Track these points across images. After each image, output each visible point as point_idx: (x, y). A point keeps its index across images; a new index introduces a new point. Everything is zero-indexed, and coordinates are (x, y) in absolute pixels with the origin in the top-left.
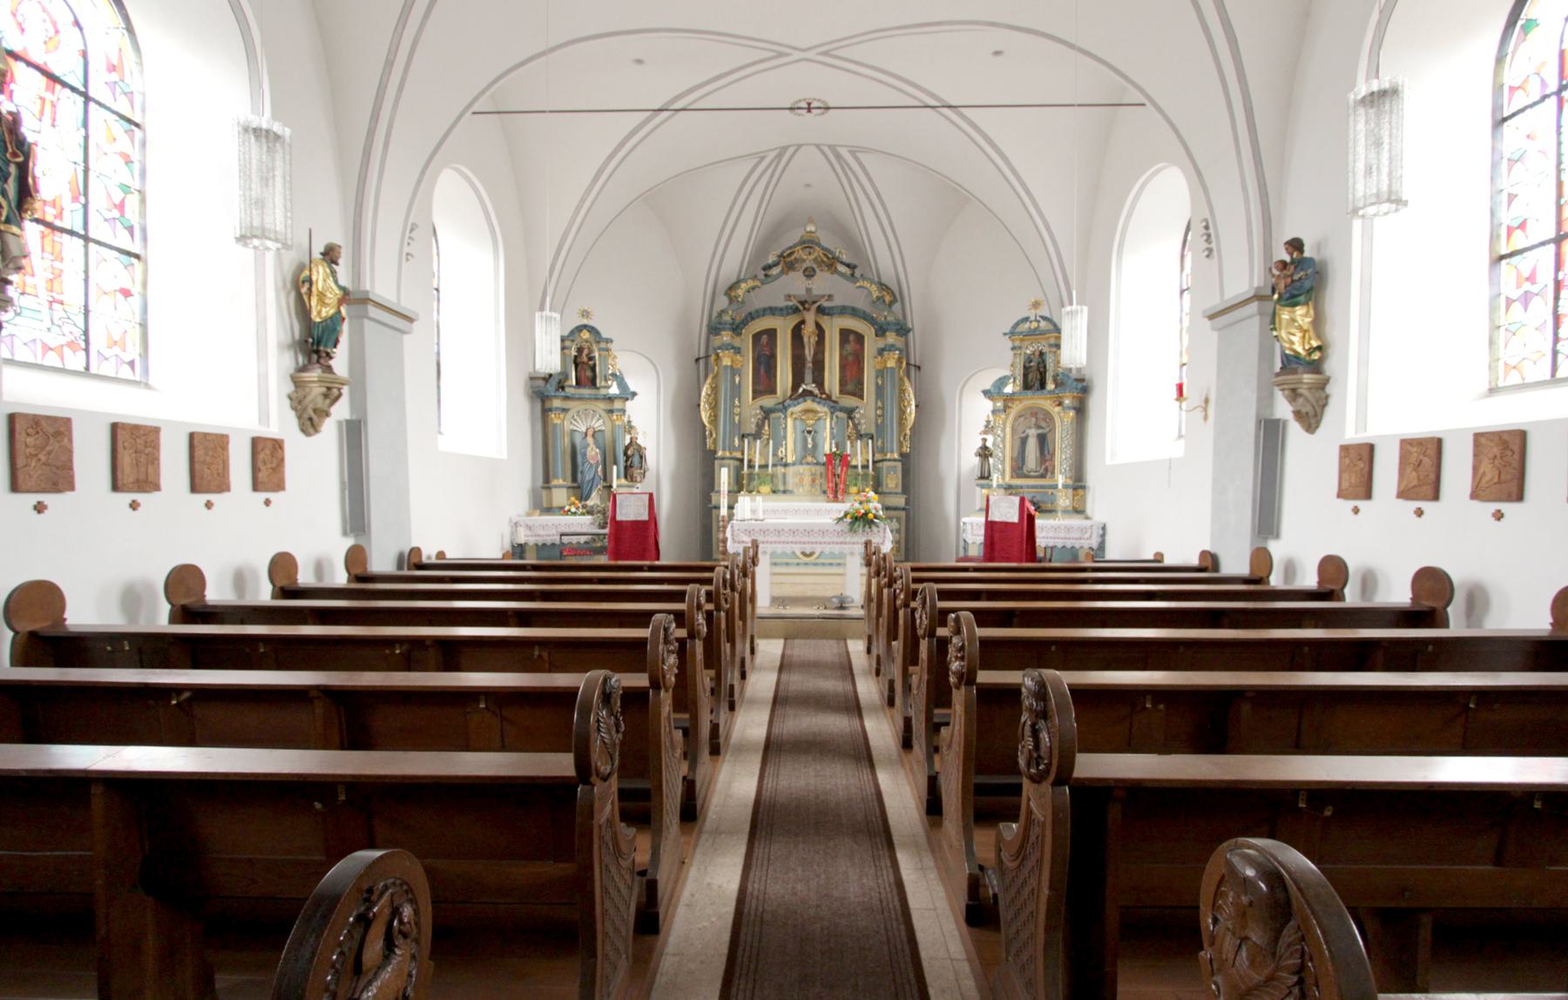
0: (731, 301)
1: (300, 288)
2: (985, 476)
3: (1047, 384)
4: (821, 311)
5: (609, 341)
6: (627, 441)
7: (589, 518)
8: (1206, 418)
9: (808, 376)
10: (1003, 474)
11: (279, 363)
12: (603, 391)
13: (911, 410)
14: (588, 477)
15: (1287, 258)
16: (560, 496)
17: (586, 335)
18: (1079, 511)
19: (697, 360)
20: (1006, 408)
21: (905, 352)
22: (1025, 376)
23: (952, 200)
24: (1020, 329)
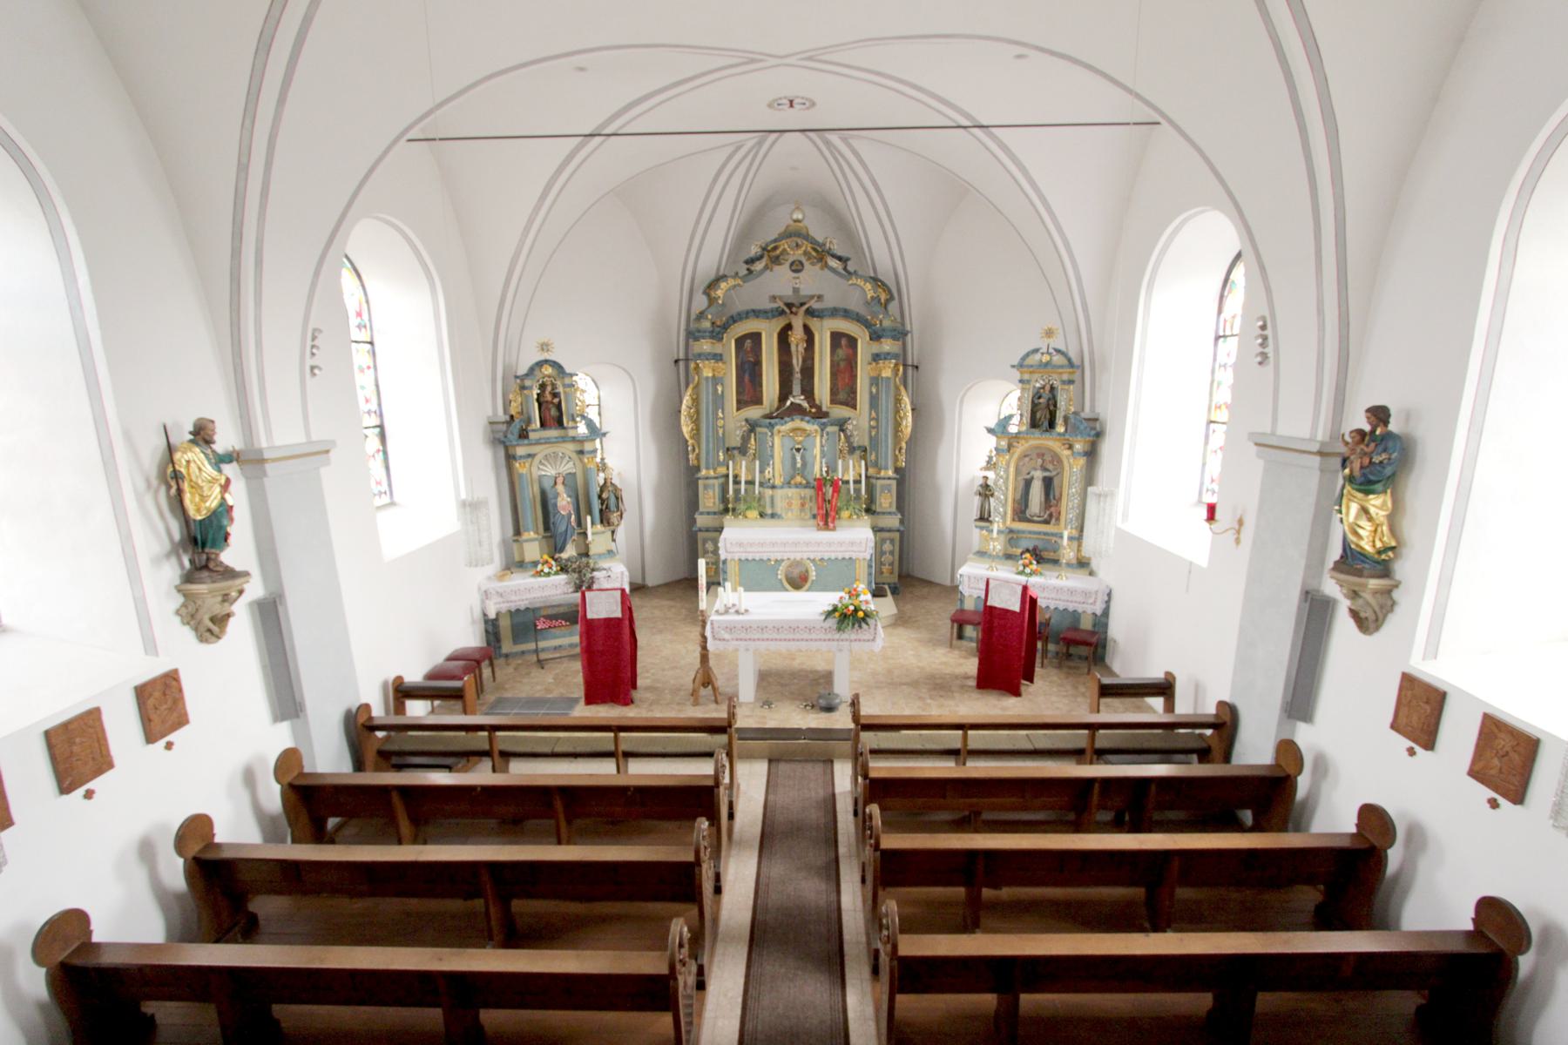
0: (712, 301)
1: (172, 478)
2: (984, 518)
3: (1062, 418)
4: (810, 313)
5: (571, 375)
6: (602, 482)
7: (563, 577)
8: (1238, 541)
9: (797, 388)
10: (1004, 516)
11: (162, 578)
12: (571, 433)
13: (908, 422)
14: (562, 528)
15: (1367, 428)
16: (533, 549)
17: (548, 370)
18: (1083, 564)
19: (676, 361)
20: (1010, 446)
21: (902, 359)
22: (1033, 413)
23: (954, 194)
24: (1029, 361)
